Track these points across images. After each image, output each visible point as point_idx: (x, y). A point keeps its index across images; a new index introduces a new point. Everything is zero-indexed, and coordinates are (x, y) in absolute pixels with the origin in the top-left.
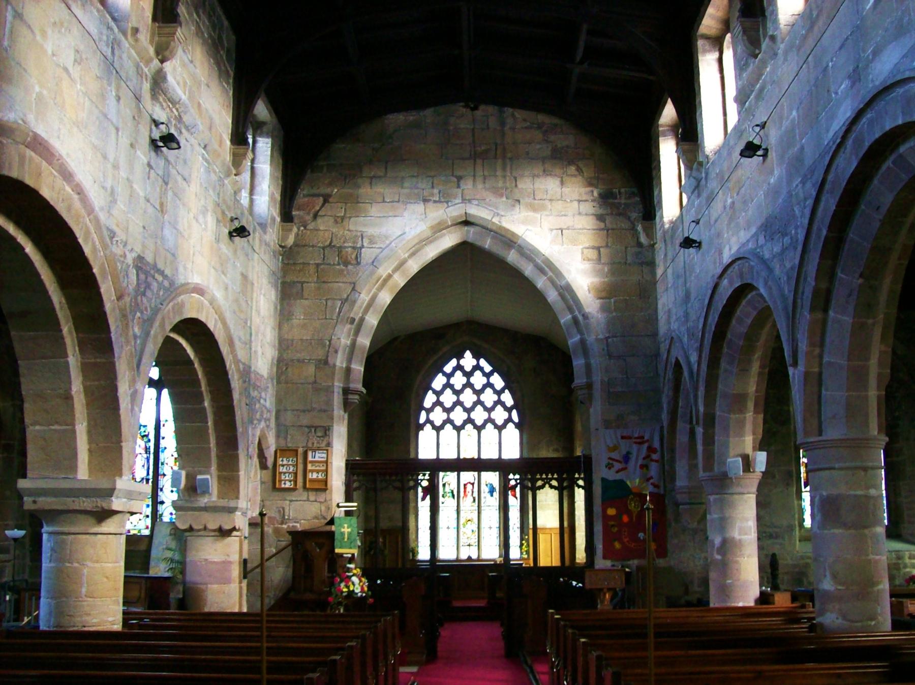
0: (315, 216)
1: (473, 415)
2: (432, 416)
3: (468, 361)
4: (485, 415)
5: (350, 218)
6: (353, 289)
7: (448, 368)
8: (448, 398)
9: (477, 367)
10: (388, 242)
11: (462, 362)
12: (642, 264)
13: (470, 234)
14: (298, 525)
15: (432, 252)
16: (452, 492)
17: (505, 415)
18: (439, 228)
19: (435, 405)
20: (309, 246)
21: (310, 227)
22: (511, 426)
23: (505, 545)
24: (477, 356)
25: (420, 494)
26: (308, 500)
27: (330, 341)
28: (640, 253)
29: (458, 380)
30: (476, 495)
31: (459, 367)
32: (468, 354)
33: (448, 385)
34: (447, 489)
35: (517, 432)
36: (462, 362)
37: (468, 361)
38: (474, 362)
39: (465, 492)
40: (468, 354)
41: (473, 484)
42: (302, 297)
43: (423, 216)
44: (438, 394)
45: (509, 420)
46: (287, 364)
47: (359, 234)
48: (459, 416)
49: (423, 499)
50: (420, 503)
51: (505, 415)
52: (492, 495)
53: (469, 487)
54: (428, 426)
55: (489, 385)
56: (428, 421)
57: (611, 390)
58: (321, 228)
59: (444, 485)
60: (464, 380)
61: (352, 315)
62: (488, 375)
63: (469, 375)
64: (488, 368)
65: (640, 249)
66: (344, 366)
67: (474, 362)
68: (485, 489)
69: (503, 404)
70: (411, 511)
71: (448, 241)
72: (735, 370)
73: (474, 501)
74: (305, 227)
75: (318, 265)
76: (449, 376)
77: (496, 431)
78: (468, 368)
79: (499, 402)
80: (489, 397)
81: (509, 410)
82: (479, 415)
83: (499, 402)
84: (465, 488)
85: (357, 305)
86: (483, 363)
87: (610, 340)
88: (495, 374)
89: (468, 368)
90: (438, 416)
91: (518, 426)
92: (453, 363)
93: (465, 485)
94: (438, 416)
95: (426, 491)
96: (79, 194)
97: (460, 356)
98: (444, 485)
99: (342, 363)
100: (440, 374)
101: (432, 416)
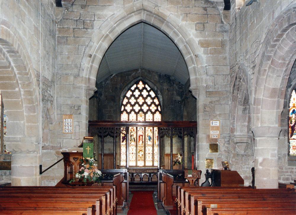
0: (72, 5)
1: (143, 108)
2: (126, 108)
3: (141, 85)
4: (147, 108)
5: (89, 6)
6: (91, 40)
7: (133, 88)
8: (133, 101)
9: (144, 88)
10: (106, 18)
11: (139, 86)
12: (223, 32)
13: (143, 16)
14: (67, 150)
15: (127, 24)
16: (134, 139)
17: (155, 108)
18: (131, 13)
19: (127, 103)
20: (70, 19)
21: (70, 10)
22: (158, 113)
23: (246, 137)
24: (144, 83)
25: (122, 140)
26: (71, 139)
27: (80, 65)
28: (222, 26)
29: (137, 93)
30: (143, 140)
31: (137, 88)
32: (141, 83)
33: (133, 95)
34: (132, 138)
35: (160, 115)
36: (139, 86)
37: (141, 85)
38: (143, 86)
39: (139, 139)
40: (141, 83)
41: (142, 136)
42: (67, 44)
43: (123, 6)
44: (129, 99)
45: (157, 110)
46: (60, 76)
47: (93, 14)
48: (137, 108)
49: (123, 142)
50: (122, 144)
51: (155, 108)
52: (150, 141)
53: (141, 137)
54: (125, 113)
55: (149, 95)
56: (125, 110)
57: (207, 90)
58: (75, 11)
59: (131, 136)
60: (139, 93)
61: (90, 53)
62: (149, 92)
63: (141, 91)
64: (149, 89)
65: (222, 25)
66: (87, 77)
67: (143, 86)
68: (147, 138)
69: (155, 104)
70: (118, 146)
71: (135, 19)
72: (275, 76)
73: (143, 142)
74: (68, 10)
75: (74, 29)
76: (133, 91)
77: (152, 114)
78: (141, 88)
79: (153, 103)
80: (149, 101)
81: (157, 106)
82: (145, 108)
83: (153, 103)
84: (139, 137)
85: (93, 48)
86: (147, 86)
87: (207, 67)
88: (152, 91)
89: (141, 88)
90: (129, 108)
91: (160, 113)
92: (135, 86)
93: (139, 136)
94: (129, 108)
95: (124, 138)
96: (38, 80)
97: (137, 83)
98: (131, 136)
99: (86, 75)
100: (130, 91)
101: (126, 108)
